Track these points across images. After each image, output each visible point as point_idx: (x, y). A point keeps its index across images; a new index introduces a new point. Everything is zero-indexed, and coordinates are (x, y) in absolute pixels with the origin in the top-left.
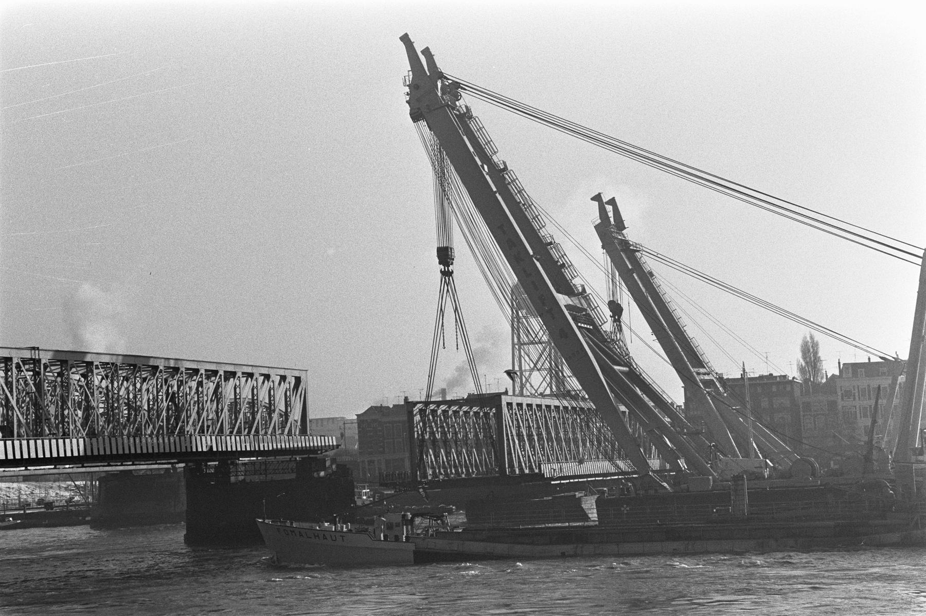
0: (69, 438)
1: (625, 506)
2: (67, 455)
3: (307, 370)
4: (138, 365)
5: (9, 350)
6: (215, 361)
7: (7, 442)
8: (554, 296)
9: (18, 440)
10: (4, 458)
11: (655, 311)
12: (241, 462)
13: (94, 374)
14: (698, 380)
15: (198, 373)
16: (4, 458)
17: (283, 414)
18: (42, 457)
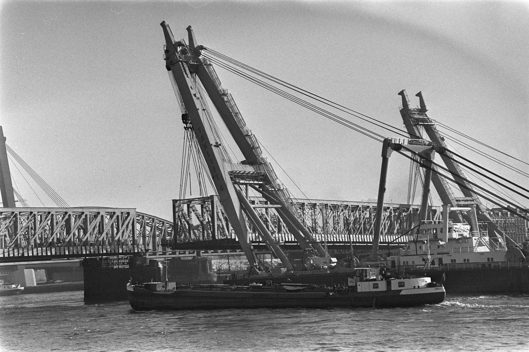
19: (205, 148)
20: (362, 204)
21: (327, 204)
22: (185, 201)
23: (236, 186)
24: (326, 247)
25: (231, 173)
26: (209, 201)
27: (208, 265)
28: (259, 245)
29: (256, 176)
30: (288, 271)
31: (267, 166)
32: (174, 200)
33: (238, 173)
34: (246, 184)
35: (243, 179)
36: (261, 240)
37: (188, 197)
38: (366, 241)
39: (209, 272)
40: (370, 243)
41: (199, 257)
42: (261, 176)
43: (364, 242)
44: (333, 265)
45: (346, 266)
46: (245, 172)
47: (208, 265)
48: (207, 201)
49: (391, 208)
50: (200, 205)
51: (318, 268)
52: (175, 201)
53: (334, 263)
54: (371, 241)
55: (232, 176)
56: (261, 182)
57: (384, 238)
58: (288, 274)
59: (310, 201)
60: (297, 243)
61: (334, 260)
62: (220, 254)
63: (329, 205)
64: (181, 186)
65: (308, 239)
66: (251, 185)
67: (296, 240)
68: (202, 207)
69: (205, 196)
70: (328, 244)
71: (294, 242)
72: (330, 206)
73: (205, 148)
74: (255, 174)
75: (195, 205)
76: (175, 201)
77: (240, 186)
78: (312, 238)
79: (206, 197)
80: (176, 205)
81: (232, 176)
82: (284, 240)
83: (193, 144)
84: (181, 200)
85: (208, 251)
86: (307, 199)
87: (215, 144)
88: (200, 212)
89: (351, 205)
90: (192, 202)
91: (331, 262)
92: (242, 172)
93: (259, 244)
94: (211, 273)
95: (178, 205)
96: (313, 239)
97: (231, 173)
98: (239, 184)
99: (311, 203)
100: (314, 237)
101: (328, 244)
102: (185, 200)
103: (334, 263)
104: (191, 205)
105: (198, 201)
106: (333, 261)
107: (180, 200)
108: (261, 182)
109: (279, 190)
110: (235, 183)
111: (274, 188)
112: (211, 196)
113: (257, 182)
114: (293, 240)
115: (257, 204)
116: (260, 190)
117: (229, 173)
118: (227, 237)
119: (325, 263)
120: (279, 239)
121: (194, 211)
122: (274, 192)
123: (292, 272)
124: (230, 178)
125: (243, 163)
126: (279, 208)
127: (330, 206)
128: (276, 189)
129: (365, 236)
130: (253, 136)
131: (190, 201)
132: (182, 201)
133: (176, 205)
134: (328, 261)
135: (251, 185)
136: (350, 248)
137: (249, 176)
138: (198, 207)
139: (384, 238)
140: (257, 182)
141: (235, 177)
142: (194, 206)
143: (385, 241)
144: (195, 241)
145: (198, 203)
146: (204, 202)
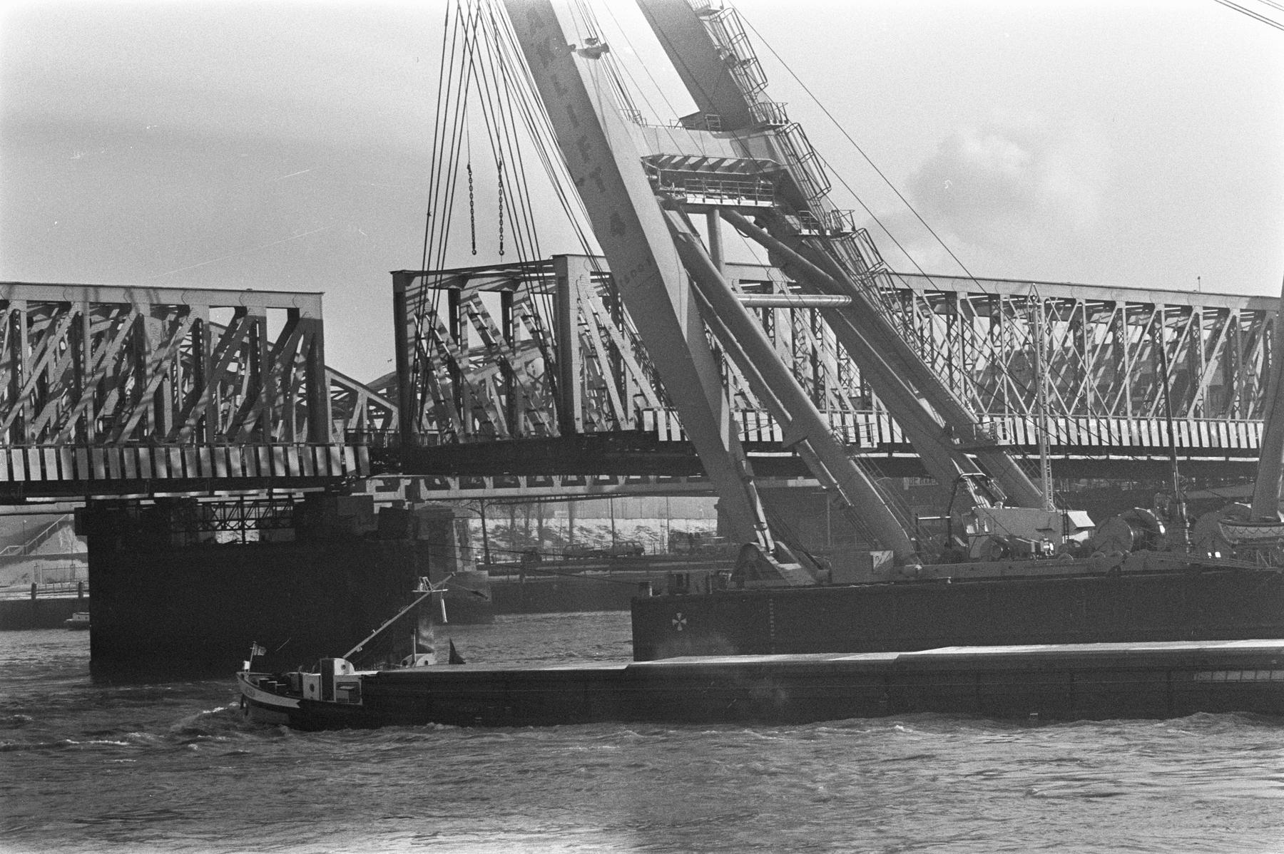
0: (1146, 419)
1: (684, 621)
2: (884, 442)
3: (321, 293)
4: (1078, 301)
5: (292, 296)
6: (239, 289)
7: (1080, 420)
8: (899, 651)
9: (1009, 417)
10: (6, 479)
11: (441, 610)
12: (216, 499)
13: (1201, 327)
14: (1013, 461)
15: (1191, 313)
16: (56, 479)
17: (437, 432)
18: (901, 441)
19: (545, 64)
20: (1013, 289)
21: (997, 296)
22: (444, 277)
23: (674, 215)
24: (1046, 469)
25: (653, 164)
26: (531, 279)
27: (456, 538)
28: (890, 459)
29: (747, 178)
30: (898, 561)
31: (787, 134)
32: (401, 272)
33: (676, 166)
34: (708, 210)
35: (695, 188)
36: (778, 437)
37: (458, 259)
38: (1146, 443)
39: (459, 564)
40: (1248, 452)
41: (418, 506)
42: (766, 176)
43: (1140, 450)
44: (1082, 537)
45: (1136, 541)
46: (705, 159)
47: (456, 538)
48: (525, 280)
49: (1121, 305)
50: (499, 294)
51: (1011, 549)
52: (402, 278)
53: (1081, 529)
54: (1253, 445)
55: (655, 177)
56: (767, 204)
57: (1214, 432)
58: (900, 578)
59: (935, 281)
60: (794, 452)
61: (1080, 518)
62: (527, 493)
63: (1003, 299)
64: (429, 214)
65: (958, 434)
66: (726, 212)
67: (908, 441)
68: (507, 302)
69: (530, 259)
70: (1053, 457)
71: (902, 448)
72: (964, 302)
73: (545, 64)
74: (743, 169)
75: (480, 293)
76: (402, 278)
77: (691, 216)
78: (979, 432)
79: (534, 263)
80: (408, 294)
81: (655, 177)
82: (877, 440)
83: (481, 38)
84: (429, 273)
85: (484, 478)
86: (919, 275)
87: (586, 46)
88: (497, 320)
89: (1088, 301)
90: (471, 283)
91: (1068, 526)
92: (692, 161)
93: (1227, 458)
94: (467, 569)
95: (417, 291)
96: (980, 434)
97: (653, 164)
98: (686, 209)
99: (939, 291)
100: (986, 428)
101: (1053, 457)
102: (443, 272)
103: (1081, 529)
104: (464, 294)
105: (489, 280)
106: (1079, 525)
107: (422, 273)
108: (767, 204)
109: (838, 233)
110: (667, 205)
111: (817, 226)
112: (554, 256)
113: (751, 203)
114: (898, 440)
115: (782, 292)
116: (762, 234)
117: (643, 164)
118: (617, 425)
119: (1046, 530)
120: (857, 434)
121: (472, 316)
122: (819, 245)
123: (919, 567)
124: (647, 183)
125: (689, 122)
126: (842, 307)
127: (964, 302)
128: (828, 233)
129: (1143, 423)
130: (727, 12)
131: (462, 276)
132: (432, 278)
133: (408, 294)
134: (1057, 525)
135: (726, 212)
136: (1169, 478)
137: (717, 176)
138: (491, 302)
139: (1214, 432)
140: (751, 203)
141: (665, 183)
142: (477, 296)
143: (1215, 445)
144: (473, 440)
145: (487, 287)
146: (515, 284)
